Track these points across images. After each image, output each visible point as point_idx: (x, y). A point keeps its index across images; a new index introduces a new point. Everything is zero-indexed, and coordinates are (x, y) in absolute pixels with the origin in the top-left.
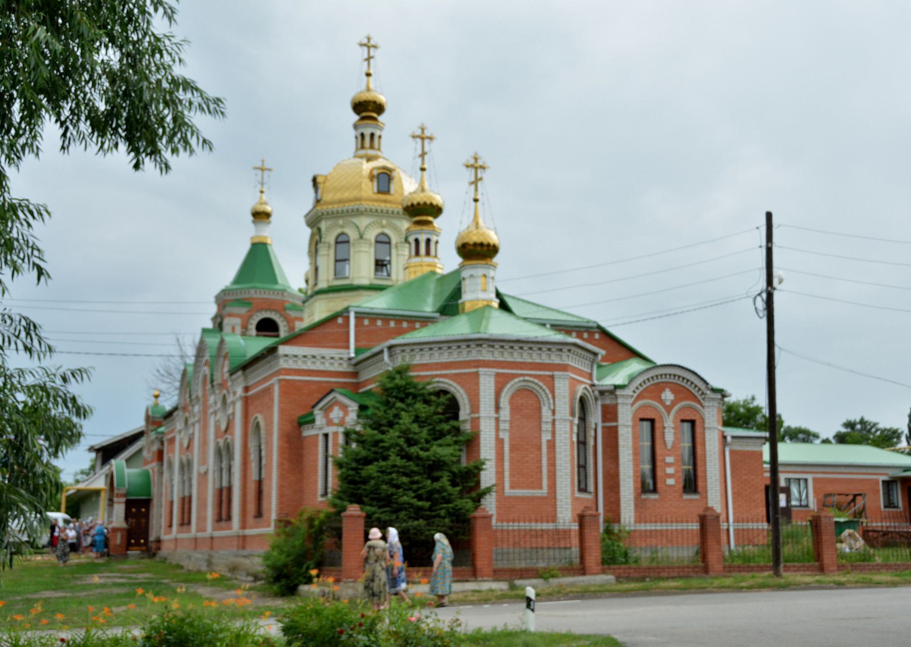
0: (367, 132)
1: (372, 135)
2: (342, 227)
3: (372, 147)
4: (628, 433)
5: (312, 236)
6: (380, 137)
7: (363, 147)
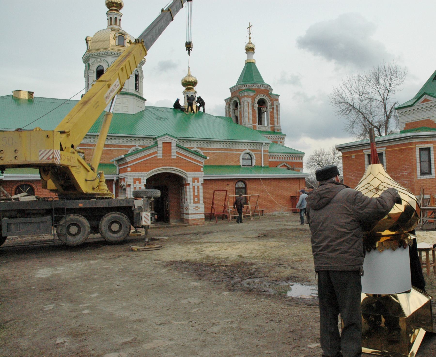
0: (113, 17)
1: (116, 18)
2: (99, 62)
3: (116, 24)
4: (317, 326)
5: (86, 67)
6: (120, 20)
7: (111, 24)
